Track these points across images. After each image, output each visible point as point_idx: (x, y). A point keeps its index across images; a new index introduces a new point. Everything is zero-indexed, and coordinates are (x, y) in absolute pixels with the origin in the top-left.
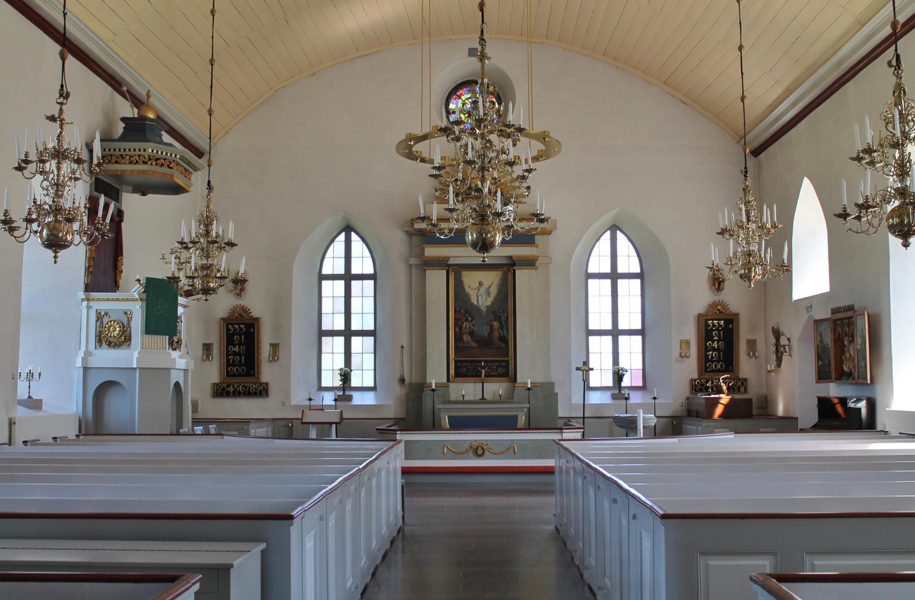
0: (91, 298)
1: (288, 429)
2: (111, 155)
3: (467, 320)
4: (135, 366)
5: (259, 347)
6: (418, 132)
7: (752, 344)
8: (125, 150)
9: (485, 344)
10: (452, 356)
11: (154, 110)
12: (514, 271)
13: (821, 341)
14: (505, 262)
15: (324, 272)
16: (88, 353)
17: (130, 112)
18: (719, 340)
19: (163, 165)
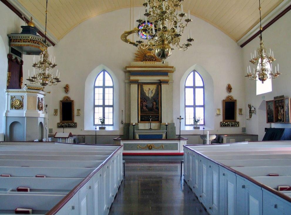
1: (80, 140)
2: (17, 39)
3: (145, 101)
4: (24, 116)
5: (73, 110)
7: (241, 110)
8: (22, 37)
9: (151, 110)
10: (140, 114)
11: (34, 24)
12: (161, 85)
13: (269, 108)
15: (96, 85)
16: (7, 111)
17: (24, 24)
18: (230, 110)
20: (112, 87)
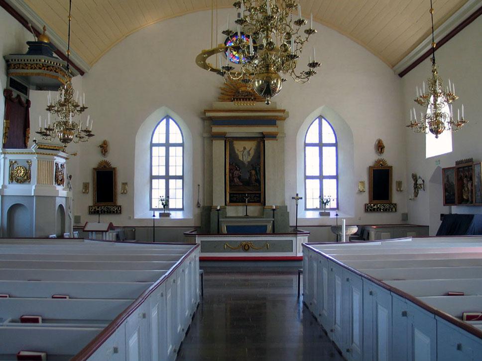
0: (6, 152)
1: (129, 235)
2: (19, 64)
4: (33, 195)
6: (209, 48)
7: (399, 184)
8: (28, 60)
11: (48, 38)
13: (448, 181)
14: (259, 136)
17: (32, 38)
18: (381, 184)
19: (51, 70)
20: (182, 145)
